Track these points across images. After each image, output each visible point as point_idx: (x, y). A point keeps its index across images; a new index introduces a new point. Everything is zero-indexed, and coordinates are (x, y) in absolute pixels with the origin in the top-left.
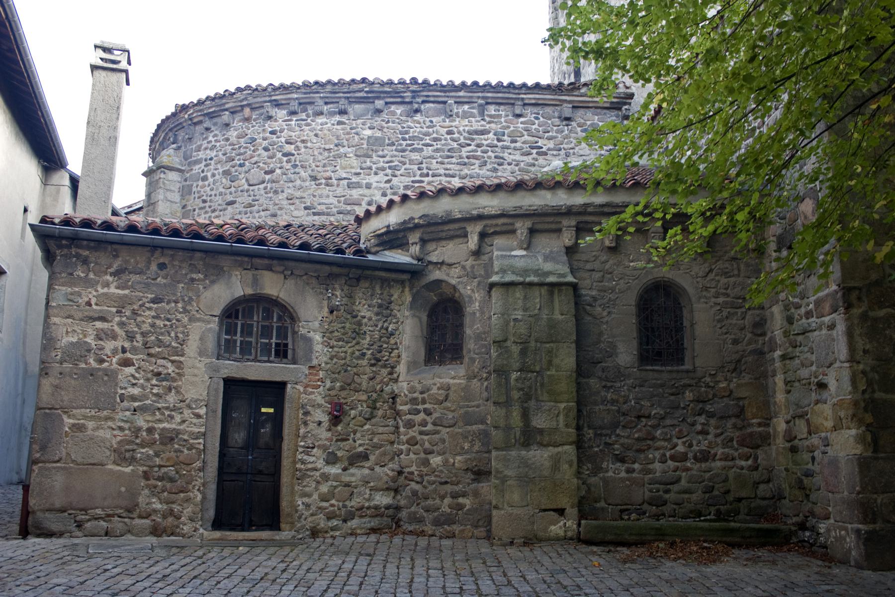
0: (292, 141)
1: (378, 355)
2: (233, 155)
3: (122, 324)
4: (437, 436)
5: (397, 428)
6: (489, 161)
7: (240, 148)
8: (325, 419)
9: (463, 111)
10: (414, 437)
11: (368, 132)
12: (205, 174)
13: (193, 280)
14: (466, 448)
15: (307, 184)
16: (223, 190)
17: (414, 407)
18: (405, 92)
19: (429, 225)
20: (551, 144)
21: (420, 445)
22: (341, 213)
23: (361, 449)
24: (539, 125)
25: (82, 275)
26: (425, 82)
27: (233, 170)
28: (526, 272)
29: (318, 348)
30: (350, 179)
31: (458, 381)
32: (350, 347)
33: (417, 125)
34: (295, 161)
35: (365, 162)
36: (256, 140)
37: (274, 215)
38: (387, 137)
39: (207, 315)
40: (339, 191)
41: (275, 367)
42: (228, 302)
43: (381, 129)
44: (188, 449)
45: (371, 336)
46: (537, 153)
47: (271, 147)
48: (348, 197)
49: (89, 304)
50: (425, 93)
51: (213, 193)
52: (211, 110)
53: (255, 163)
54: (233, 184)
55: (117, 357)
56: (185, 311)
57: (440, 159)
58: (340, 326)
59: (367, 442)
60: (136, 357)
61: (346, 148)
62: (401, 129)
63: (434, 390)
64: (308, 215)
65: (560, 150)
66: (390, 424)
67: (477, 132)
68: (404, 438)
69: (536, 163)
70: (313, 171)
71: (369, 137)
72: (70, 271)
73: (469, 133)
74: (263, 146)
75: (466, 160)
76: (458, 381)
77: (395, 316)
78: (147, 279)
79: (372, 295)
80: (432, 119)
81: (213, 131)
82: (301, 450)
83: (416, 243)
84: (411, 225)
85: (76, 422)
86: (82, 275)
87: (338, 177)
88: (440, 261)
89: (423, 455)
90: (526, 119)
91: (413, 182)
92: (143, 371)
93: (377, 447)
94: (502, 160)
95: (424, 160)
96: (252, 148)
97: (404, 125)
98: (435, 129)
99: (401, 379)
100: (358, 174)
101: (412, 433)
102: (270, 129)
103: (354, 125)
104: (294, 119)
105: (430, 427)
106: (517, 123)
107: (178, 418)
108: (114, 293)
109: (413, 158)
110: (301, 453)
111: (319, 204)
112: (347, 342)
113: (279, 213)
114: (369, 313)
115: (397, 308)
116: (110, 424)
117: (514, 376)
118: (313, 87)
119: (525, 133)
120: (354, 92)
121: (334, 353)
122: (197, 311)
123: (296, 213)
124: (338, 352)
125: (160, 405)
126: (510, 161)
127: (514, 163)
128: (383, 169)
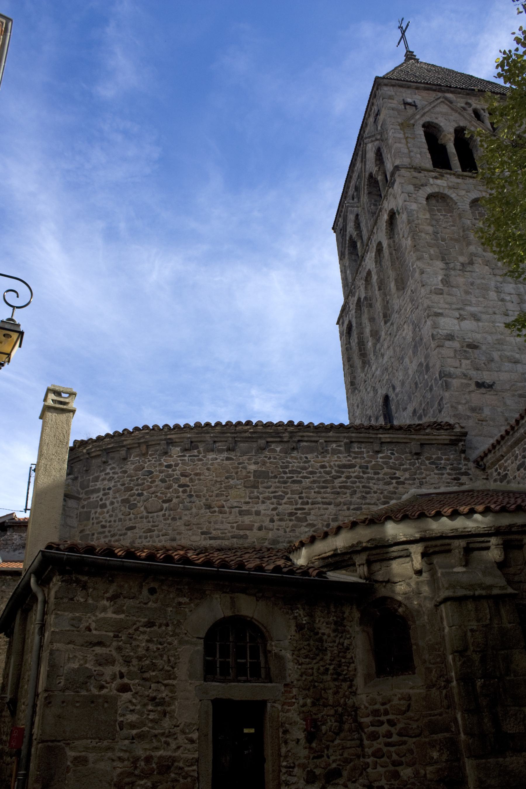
0: (187, 474)
1: (339, 670)
2: (131, 485)
3: (119, 649)
4: (404, 747)
5: (361, 740)
6: (358, 490)
7: (137, 479)
8: (301, 736)
9: (332, 449)
10: (379, 750)
11: (253, 467)
12: (103, 502)
13: (180, 604)
14: (435, 757)
15: (203, 511)
16: (123, 517)
17: (377, 718)
18: (283, 433)
19: (376, 547)
20: (407, 475)
21: (388, 757)
22: (234, 538)
23: (334, 765)
24: (394, 460)
25: (82, 600)
26: (301, 424)
27: (132, 499)
28: (471, 587)
29: (290, 666)
30: (240, 507)
31: (418, 691)
32: (315, 664)
33: (295, 461)
34: (190, 492)
35: (253, 493)
36: (152, 472)
37: (173, 540)
38: (270, 471)
39: (194, 637)
40: (231, 518)
41: (256, 687)
42: (211, 624)
43: (264, 463)
44: (185, 778)
45: (332, 652)
46: (397, 483)
47: (167, 479)
48: (240, 523)
49: (89, 629)
50: (301, 434)
51: (112, 519)
52: (110, 446)
53: (153, 493)
54: (132, 511)
55: (115, 683)
56: (174, 635)
57: (317, 490)
58: (306, 643)
59: (339, 757)
60: (133, 682)
61: (235, 480)
62: (281, 464)
63: (395, 701)
64: (205, 539)
65: (414, 479)
66: (355, 737)
67: (345, 466)
68: (369, 751)
69: (397, 491)
70: (207, 500)
71: (254, 471)
72: (71, 596)
73: (339, 466)
74: (160, 478)
75: (339, 490)
76: (418, 691)
77: (348, 632)
78: (140, 603)
79: (328, 613)
80: (307, 455)
81: (110, 464)
82: (284, 770)
83: (363, 564)
84: (359, 548)
85: (78, 754)
86: (82, 600)
87: (229, 505)
88: (386, 579)
89: (391, 768)
90: (384, 455)
91: (296, 509)
92: (140, 696)
93: (347, 761)
94: (368, 490)
95: (304, 491)
96: (150, 480)
97: (284, 461)
98: (310, 464)
99: (359, 692)
100: (248, 503)
101: (377, 745)
102: (165, 464)
103: (241, 461)
104: (187, 455)
105: (395, 738)
106: (377, 458)
107: (173, 746)
108: (111, 618)
109: (294, 488)
110: (285, 773)
111: (214, 530)
112: (313, 659)
113: (178, 537)
114: (328, 630)
115: (349, 624)
116: (110, 754)
117: (479, 683)
118: (205, 429)
119: (385, 466)
120: (240, 433)
121: (303, 670)
122: (186, 634)
123: (194, 538)
124: (306, 669)
125: (156, 732)
126: (375, 490)
127: (378, 491)
128: (269, 498)
